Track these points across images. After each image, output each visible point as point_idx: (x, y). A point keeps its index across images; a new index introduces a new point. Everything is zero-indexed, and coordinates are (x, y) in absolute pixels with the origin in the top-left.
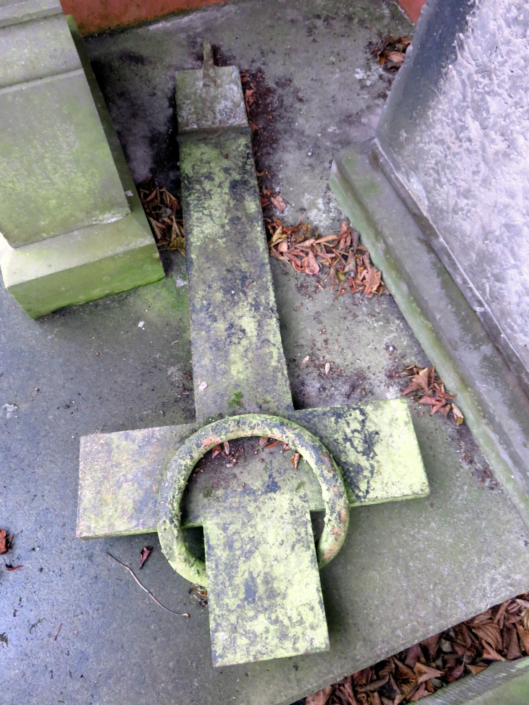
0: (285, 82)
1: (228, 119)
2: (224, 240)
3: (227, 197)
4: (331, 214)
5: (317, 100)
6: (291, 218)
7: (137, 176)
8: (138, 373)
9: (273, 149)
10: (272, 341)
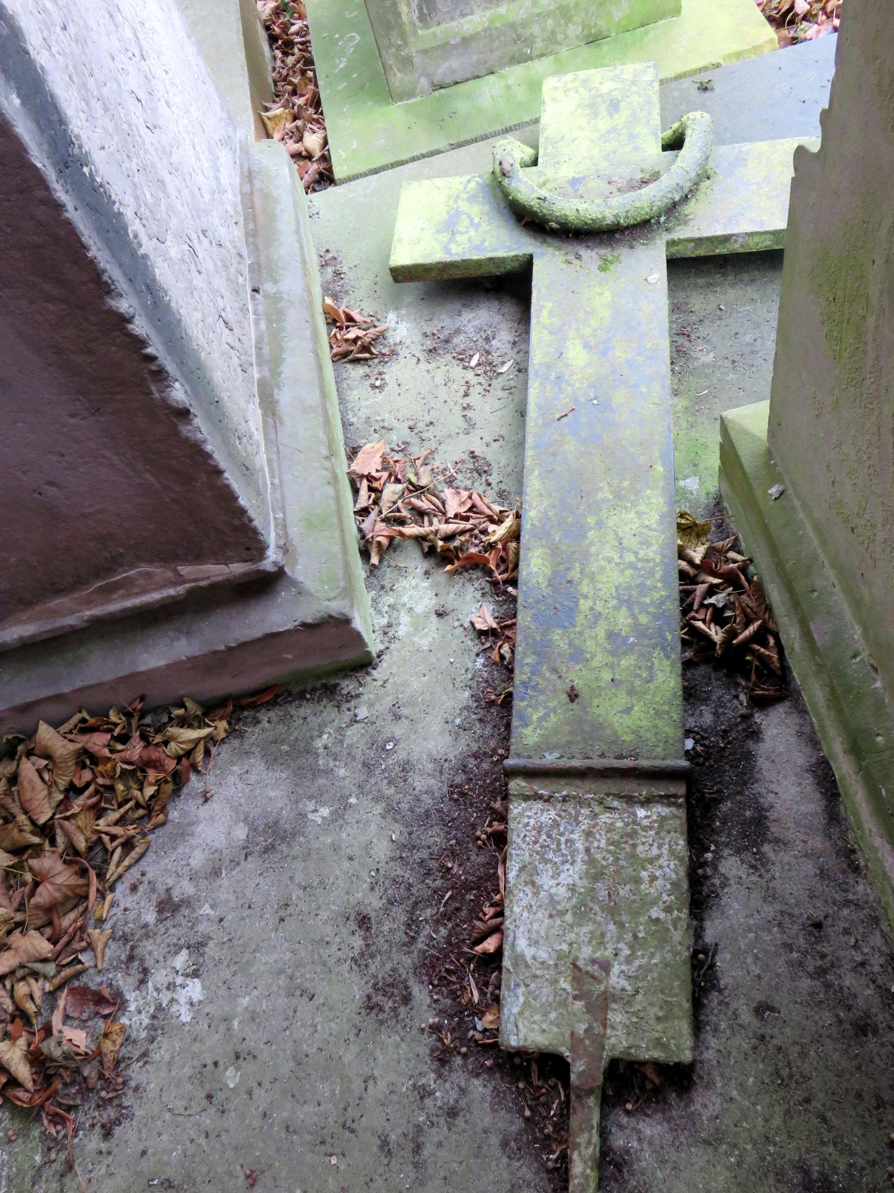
0: (384, 1000)
1: (556, 824)
2: (600, 496)
3: (585, 588)
4: (392, 601)
5: (324, 915)
6: (469, 597)
7: (793, 721)
8: (761, 354)
9: (464, 768)
10: (545, 332)
